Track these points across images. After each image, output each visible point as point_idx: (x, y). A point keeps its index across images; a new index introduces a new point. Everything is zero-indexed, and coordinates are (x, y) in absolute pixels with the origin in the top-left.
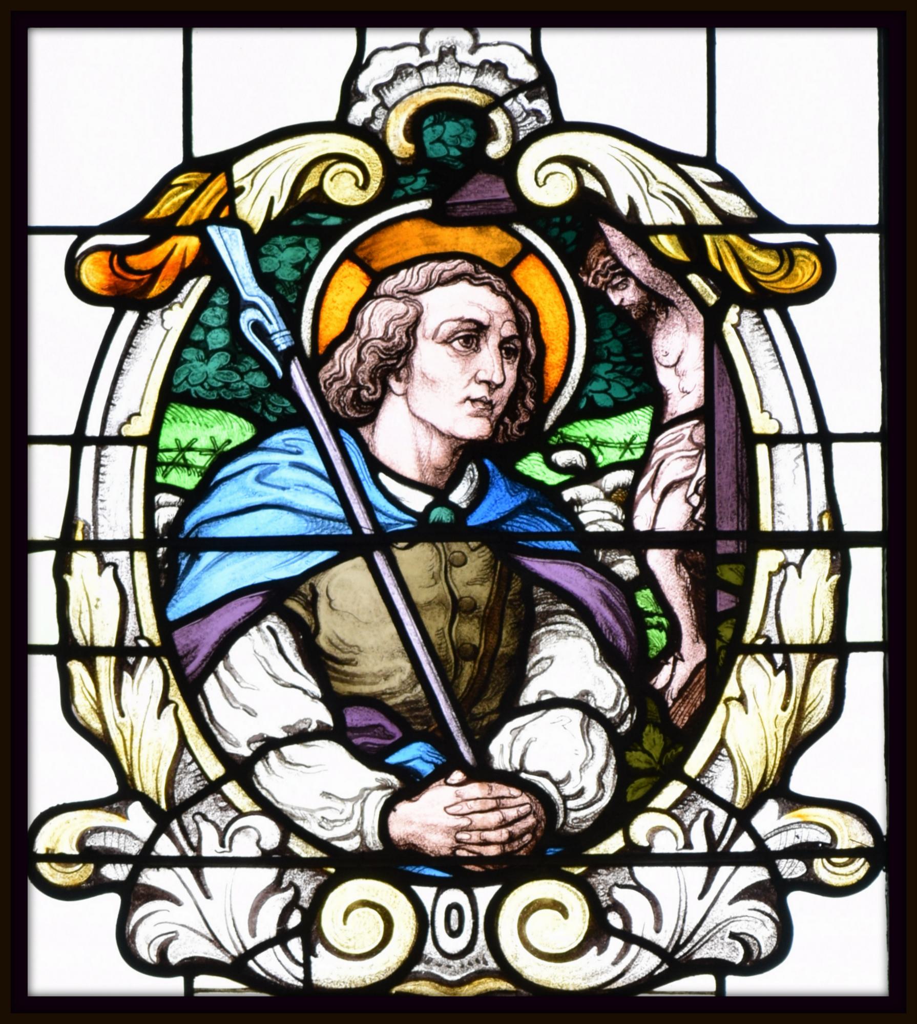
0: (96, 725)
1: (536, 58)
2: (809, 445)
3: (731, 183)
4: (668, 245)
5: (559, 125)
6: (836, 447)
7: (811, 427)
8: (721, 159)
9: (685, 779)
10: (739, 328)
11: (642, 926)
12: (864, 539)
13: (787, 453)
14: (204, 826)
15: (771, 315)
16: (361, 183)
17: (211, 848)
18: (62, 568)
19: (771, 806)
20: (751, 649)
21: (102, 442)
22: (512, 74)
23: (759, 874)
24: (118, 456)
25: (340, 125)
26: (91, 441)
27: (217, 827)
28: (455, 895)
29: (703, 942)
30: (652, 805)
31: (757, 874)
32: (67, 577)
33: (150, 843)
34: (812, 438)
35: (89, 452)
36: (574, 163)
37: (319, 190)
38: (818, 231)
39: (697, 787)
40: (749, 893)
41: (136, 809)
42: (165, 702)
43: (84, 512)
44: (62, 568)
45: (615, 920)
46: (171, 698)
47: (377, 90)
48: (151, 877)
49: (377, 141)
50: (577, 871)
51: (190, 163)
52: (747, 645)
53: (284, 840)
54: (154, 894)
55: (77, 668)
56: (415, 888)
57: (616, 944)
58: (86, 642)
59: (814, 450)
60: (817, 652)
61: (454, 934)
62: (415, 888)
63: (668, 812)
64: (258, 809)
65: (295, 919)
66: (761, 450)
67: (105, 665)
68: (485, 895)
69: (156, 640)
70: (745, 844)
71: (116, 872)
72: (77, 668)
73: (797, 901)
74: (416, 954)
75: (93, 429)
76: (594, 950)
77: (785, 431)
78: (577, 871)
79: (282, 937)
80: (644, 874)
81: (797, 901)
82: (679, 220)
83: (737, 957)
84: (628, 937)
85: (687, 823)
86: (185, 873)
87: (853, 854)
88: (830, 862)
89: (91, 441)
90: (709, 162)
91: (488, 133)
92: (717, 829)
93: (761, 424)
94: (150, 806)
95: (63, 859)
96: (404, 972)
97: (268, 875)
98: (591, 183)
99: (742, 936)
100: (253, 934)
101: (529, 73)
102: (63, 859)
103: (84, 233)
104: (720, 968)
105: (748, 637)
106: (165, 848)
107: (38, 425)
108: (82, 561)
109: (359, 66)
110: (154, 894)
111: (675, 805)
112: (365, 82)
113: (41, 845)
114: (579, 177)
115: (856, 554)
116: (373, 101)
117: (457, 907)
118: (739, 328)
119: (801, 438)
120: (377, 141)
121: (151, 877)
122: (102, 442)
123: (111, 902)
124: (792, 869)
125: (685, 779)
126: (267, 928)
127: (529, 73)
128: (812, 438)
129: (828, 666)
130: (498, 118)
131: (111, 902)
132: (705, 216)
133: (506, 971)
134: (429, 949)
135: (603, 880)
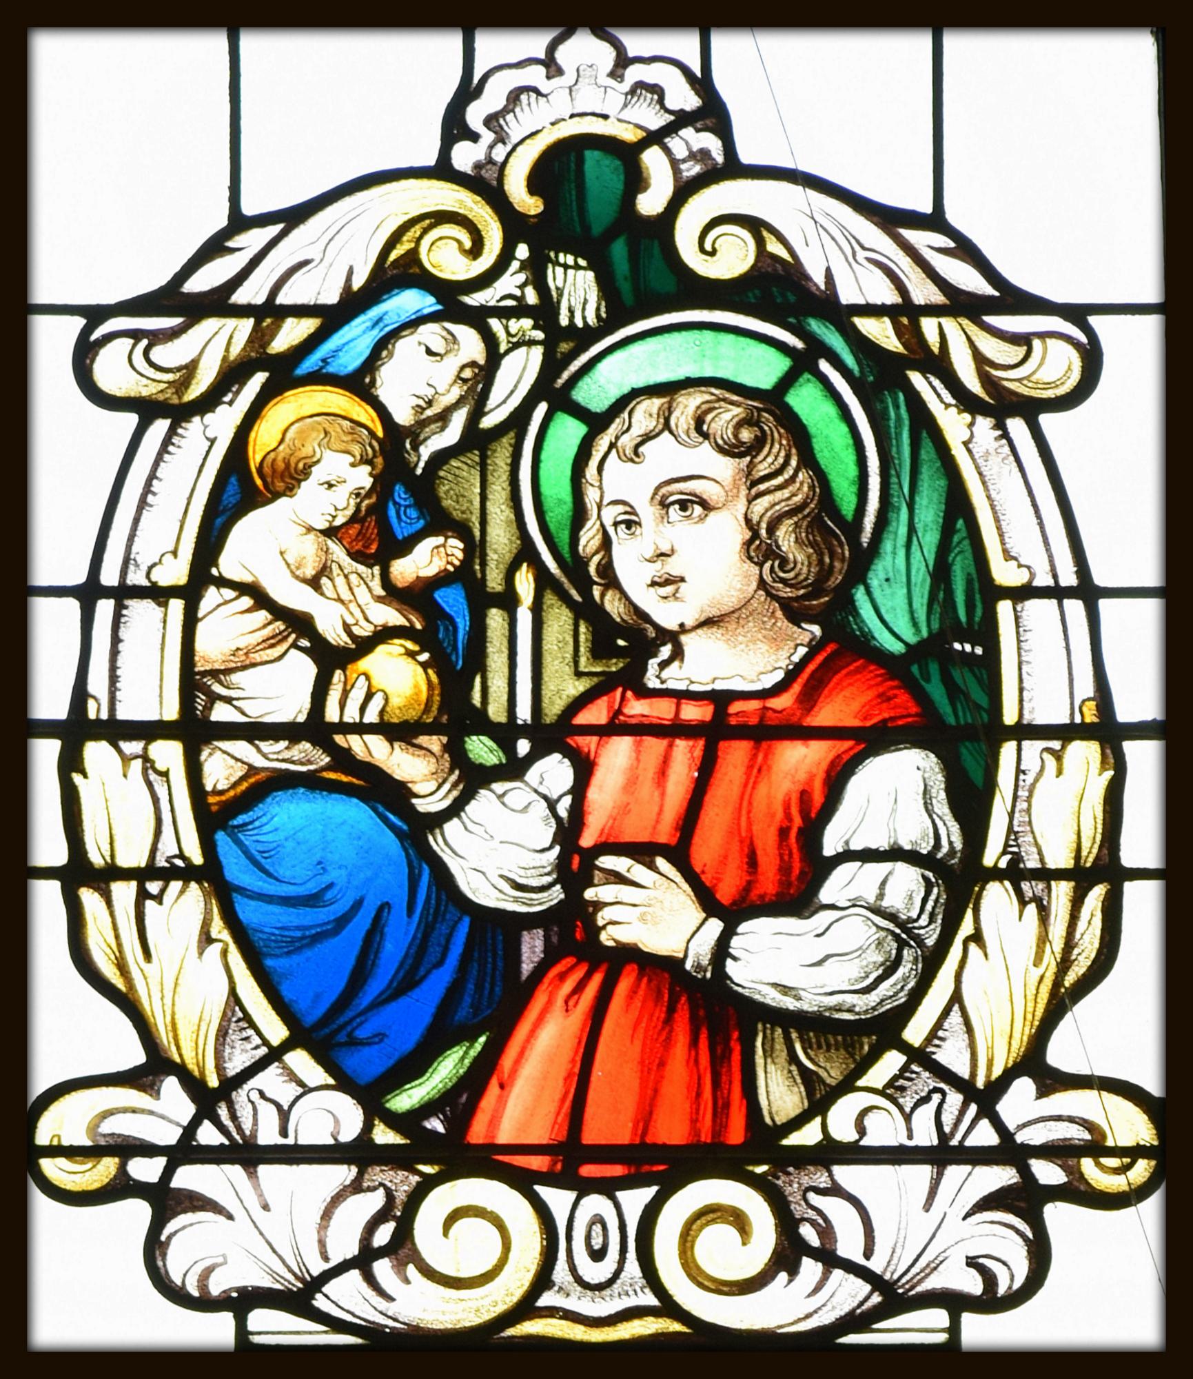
0: (120, 984)
1: (703, 83)
2: (1066, 602)
3: (966, 250)
4: (881, 332)
5: (733, 168)
6: (1104, 604)
7: (1068, 578)
8: (953, 216)
9: (904, 1047)
10: (971, 446)
11: (849, 1246)
12: (1140, 731)
13: (1039, 611)
14: (263, 1106)
15: (1016, 426)
16: (468, 244)
17: (268, 1135)
18: (71, 763)
19: (1024, 1087)
20: (996, 874)
21: (123, 593)
22: (671, 103)
23: (1002, 1176)
24: (141, 612)
25: (443, 170)
26: (108, 592)
27: (278, 1106)
28: (596, 1204)
29: (933, 1268)
30: (860, 1083)
31: (1001, 1176)
32: (77, 778)
33: (190, 1130)
34: (1070, 593)
35: (105, 608)
36: (755, 225)
37: (413, 256)
38: (1077, 314)
39: (920, 1057)
40: (988, 1203)
41: (171, 1085)
42: (206, 939)
43: (97, 683)
44: (71, 763)
45: (808, 1233)
46: (214, 935)
47: (491, 121)
48: (188, 1177)
49: (495, 196)
50: (760, 1169)
51: (239, 223)
52: (988, 869)
53: (368, 1127)
54: (197, 1202)
55: (89, 898)
56: (537, 1188)
57: (810, 1269)
58: (106, 862)
59: (1075, 608)
60: (1082, 878)
61: (598, 1255)
62: (537, 1188)
63: (881, 1093)
64: (331, 1081)
65: (383, 1235)
66: (1004, 608)
67: (124, 892)
68: (635, 1200)
69: (198, 859)
70: (985, 1135)
71: (146, 1170)
72: (89, 898)
73: (1056, 1215)
74: (543, 1280)
75: (110, 577)
76: (783, 1276)
77: (1037, 583)
78: (760, 1169)
79: (364, 1260)
80: (845, 1174)
81: (1056, 1215)
82: (890, 297)
83: (973, 1285)
84: (829, 1259)
85: (908, 1110)
86: (236, 1172)
87: (1135, 1153)
88: (1098, 1164)
89: (108, 592)
90: (936, 221)
91: (636, 181)
92: (948, 1119)
93: (1004, 574)
94: (193, 1085)
95: (72, 1152)
96: (526, 1308)
97: (344, 1173)
98: (774, 247)
99: (981, 1260)
100: (326, 1259)
101: (687, 99)
102: (72, 1152)
103: (95, 314)
104: (955, 1303)
105: (989, 860)
106: (208, 1135)
107: (42, 574)
108: (97, 753)
109: (468, 91)
110: (197, 1202)
111: (890, 1084)
112: (475, 115)
113: (43, 1137)
114: (760, 242)
115: (1129, 747)
116: (487, 136)
117: (599, 1220)
118: (971, 446)
119: (1057, 593)
120: (495, 196)
121: (188, 1177)
122: (123, 593)
123: (138, 1212)
124: (1048, 1173)
125: (904, 1047)
126: (345, 1246)
127: (687, 99)
128: (1070, 593)
129: (1097, 895)
130: (652, 158)
131: (138, 1212)
132: (923, 292)
133: (669, 1307)
134: (561, 1272)
135: (793, 1184)
